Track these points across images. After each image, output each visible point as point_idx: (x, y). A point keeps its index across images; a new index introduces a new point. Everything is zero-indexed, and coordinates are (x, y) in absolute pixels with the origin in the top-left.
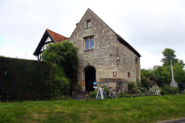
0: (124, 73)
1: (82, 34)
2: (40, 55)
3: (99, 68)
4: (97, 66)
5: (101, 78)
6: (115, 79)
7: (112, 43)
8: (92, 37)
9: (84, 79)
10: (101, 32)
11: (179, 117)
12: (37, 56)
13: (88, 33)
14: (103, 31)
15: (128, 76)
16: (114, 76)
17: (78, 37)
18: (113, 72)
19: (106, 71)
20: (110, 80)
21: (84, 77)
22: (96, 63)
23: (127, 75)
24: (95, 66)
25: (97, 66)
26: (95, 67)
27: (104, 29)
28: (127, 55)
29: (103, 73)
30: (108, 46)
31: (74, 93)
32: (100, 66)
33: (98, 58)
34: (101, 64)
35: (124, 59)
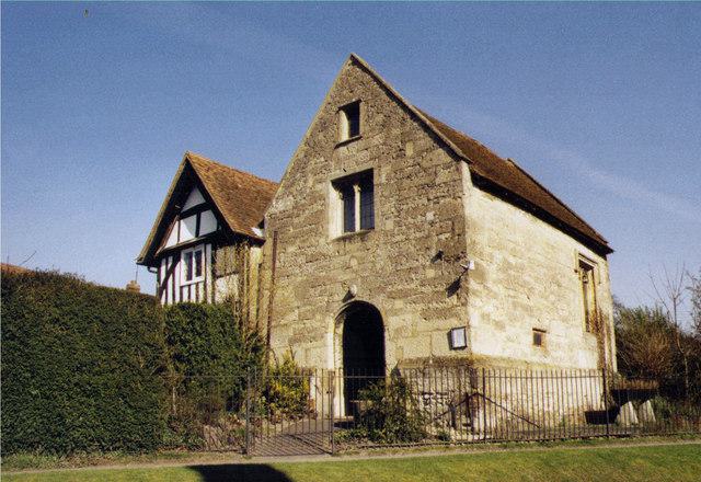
0: (510, 330)
1: (326, 168)
2: (164, 261)
3: (395, 313)
4: (388, 306)
5: (406, 356)
6: (462, 359)
7: (448, 200)
8: (365, 179)
9: (339, 364)
10: (401, 153)
11: (425, 458)
12: (155, 270)
13: (353, 160)
14: (409, 151)
15: (538, 340)
16: (452, 347)
17: (310, 183)
18: (189, 285)
19: (423, 325)
20: (440, 363)
21: (339, 349)
22: (381, 290)
23: (531, 339)
24: (379, 302)
25: (388, 306)
26: (379, 307)
27: (413, 141)
28: (529, 250)
29: (413, 336)
30: (430, 216)
31: (252, 396)
32: (399, 304)
33: (390, 269)
34: (404, 295)
35: (506, 267)
